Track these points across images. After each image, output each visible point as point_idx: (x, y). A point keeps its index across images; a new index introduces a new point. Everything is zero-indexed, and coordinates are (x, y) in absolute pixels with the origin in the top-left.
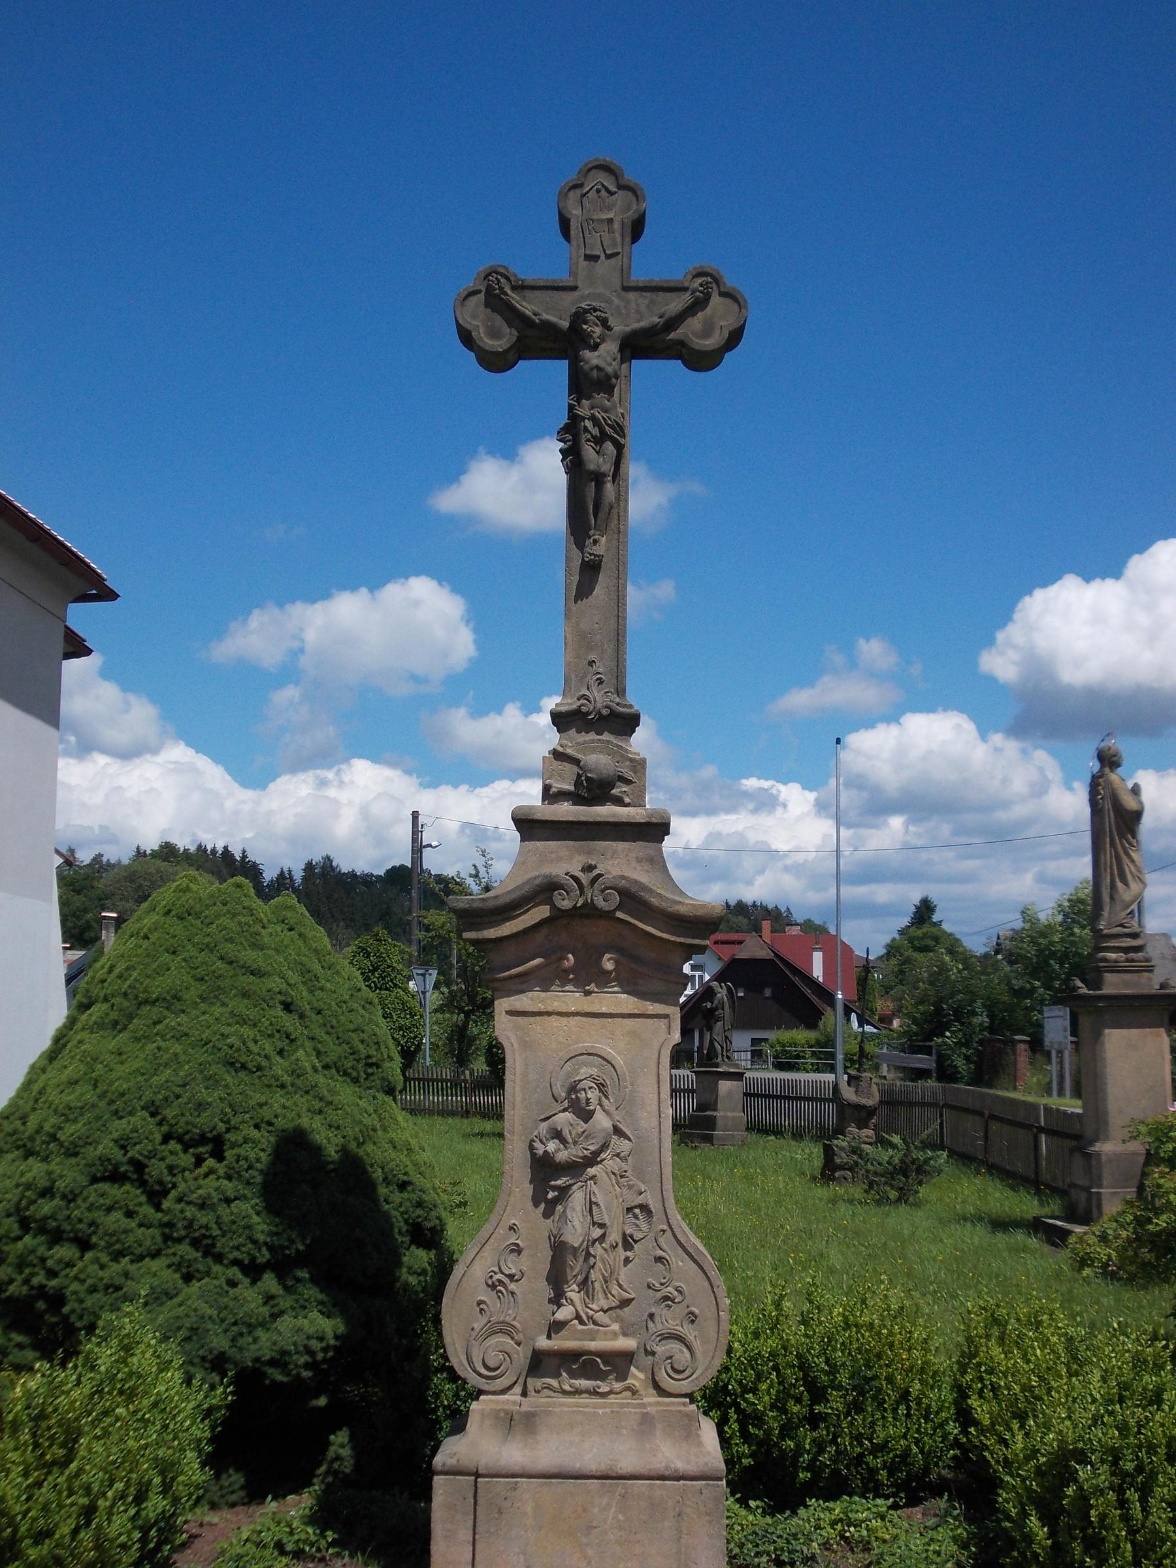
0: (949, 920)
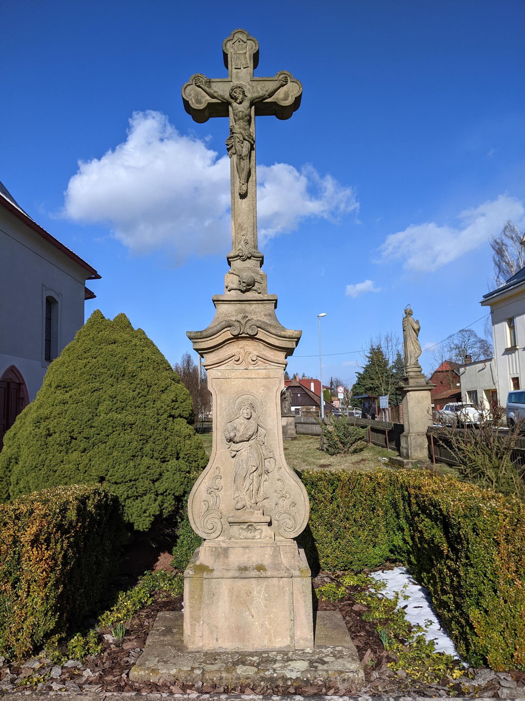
0: (167, 554)
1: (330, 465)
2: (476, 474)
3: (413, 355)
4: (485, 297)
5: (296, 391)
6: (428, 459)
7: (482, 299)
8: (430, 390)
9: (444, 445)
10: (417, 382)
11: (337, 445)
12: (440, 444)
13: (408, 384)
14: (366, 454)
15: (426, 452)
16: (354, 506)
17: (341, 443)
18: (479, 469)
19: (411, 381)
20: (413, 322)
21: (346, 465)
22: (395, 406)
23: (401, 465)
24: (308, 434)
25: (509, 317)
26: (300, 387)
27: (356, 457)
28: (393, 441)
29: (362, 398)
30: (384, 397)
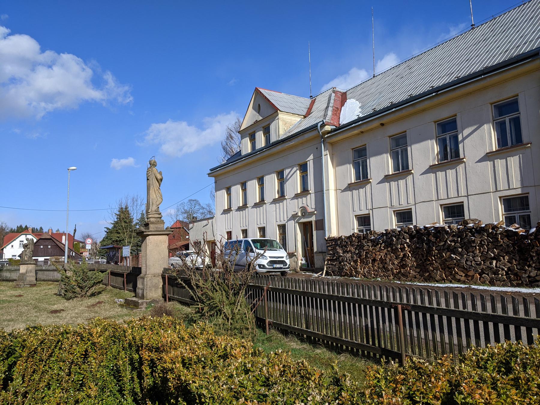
1: (63, 310)
2: (213, 312)
3: (154, 203)
4: (211, 170)
5: (47, 243)
6: (162, 299)
7: (209, 172)
8: (168, 235)
9: (182, 283)
10: (157, 228)
11: (75, 289)
12: (176, 283)
13: (148, 229)
14: (103, 297)
15: (160, 292)
16: (48, 386)
17: (79, 287)
18: (217, 307)
19: (151, 226)
20: (156, 172)
21: (80, 309)
22: (136, 253)
23: (136, 305)
24: (49, 281)
25: (228, 186)
26: (51, 239)
27: (93, 300)
28: (130, 283)
29: (107, 248)
30: (126, 247)
